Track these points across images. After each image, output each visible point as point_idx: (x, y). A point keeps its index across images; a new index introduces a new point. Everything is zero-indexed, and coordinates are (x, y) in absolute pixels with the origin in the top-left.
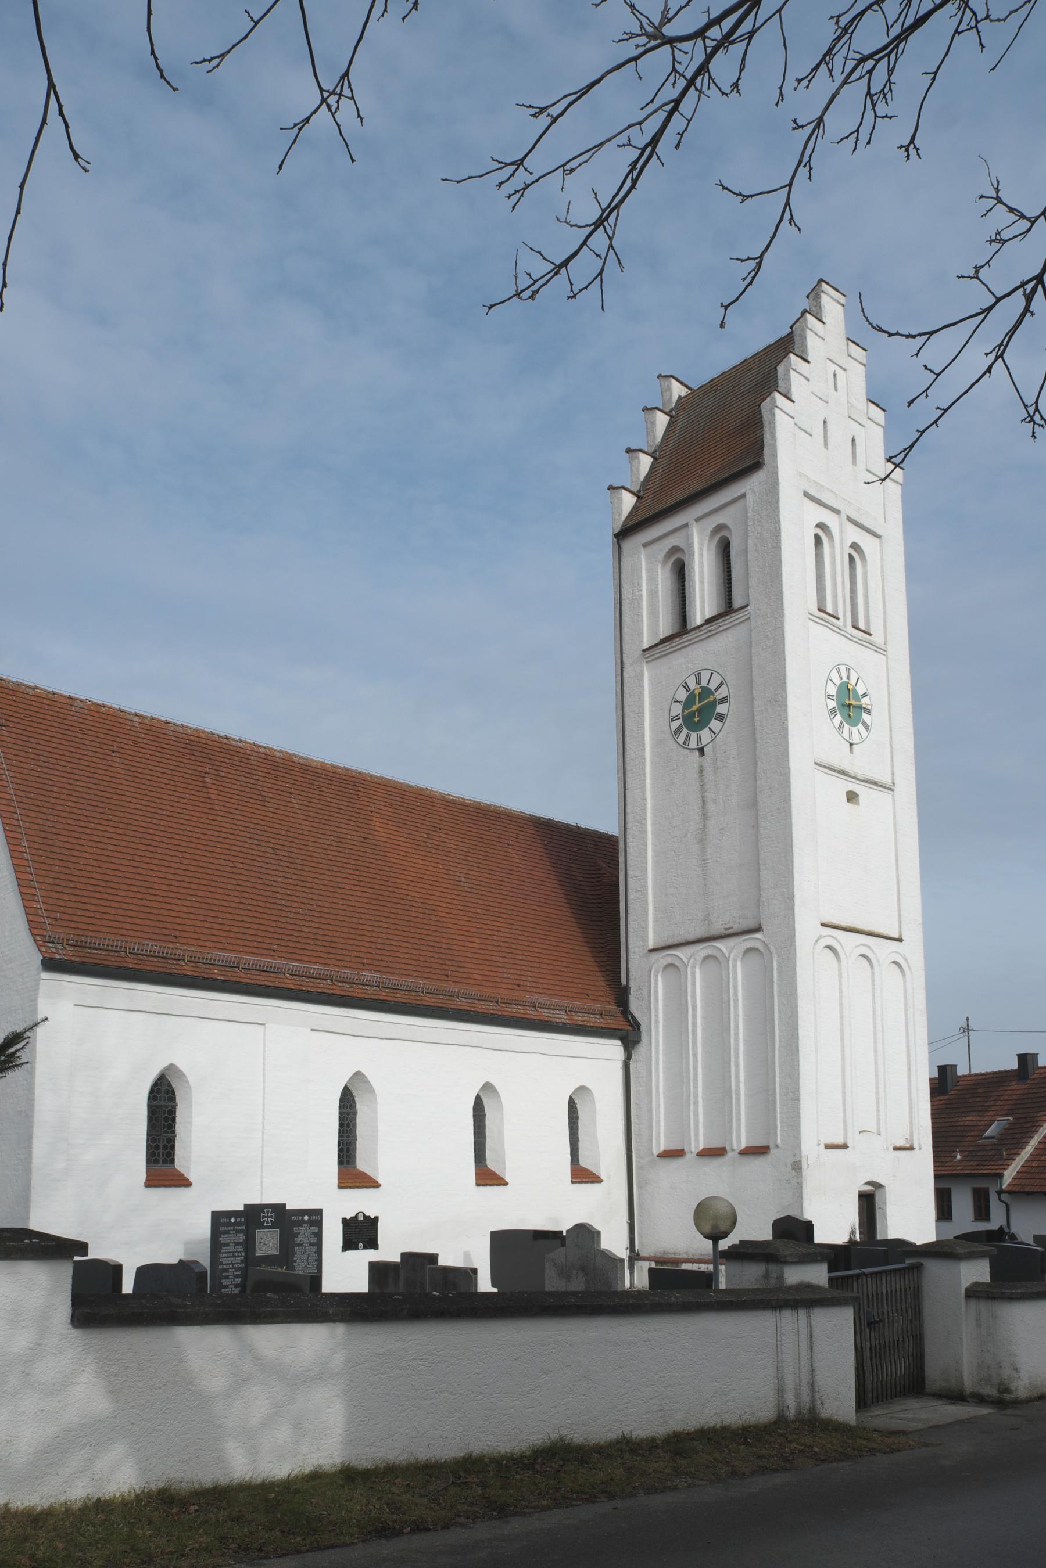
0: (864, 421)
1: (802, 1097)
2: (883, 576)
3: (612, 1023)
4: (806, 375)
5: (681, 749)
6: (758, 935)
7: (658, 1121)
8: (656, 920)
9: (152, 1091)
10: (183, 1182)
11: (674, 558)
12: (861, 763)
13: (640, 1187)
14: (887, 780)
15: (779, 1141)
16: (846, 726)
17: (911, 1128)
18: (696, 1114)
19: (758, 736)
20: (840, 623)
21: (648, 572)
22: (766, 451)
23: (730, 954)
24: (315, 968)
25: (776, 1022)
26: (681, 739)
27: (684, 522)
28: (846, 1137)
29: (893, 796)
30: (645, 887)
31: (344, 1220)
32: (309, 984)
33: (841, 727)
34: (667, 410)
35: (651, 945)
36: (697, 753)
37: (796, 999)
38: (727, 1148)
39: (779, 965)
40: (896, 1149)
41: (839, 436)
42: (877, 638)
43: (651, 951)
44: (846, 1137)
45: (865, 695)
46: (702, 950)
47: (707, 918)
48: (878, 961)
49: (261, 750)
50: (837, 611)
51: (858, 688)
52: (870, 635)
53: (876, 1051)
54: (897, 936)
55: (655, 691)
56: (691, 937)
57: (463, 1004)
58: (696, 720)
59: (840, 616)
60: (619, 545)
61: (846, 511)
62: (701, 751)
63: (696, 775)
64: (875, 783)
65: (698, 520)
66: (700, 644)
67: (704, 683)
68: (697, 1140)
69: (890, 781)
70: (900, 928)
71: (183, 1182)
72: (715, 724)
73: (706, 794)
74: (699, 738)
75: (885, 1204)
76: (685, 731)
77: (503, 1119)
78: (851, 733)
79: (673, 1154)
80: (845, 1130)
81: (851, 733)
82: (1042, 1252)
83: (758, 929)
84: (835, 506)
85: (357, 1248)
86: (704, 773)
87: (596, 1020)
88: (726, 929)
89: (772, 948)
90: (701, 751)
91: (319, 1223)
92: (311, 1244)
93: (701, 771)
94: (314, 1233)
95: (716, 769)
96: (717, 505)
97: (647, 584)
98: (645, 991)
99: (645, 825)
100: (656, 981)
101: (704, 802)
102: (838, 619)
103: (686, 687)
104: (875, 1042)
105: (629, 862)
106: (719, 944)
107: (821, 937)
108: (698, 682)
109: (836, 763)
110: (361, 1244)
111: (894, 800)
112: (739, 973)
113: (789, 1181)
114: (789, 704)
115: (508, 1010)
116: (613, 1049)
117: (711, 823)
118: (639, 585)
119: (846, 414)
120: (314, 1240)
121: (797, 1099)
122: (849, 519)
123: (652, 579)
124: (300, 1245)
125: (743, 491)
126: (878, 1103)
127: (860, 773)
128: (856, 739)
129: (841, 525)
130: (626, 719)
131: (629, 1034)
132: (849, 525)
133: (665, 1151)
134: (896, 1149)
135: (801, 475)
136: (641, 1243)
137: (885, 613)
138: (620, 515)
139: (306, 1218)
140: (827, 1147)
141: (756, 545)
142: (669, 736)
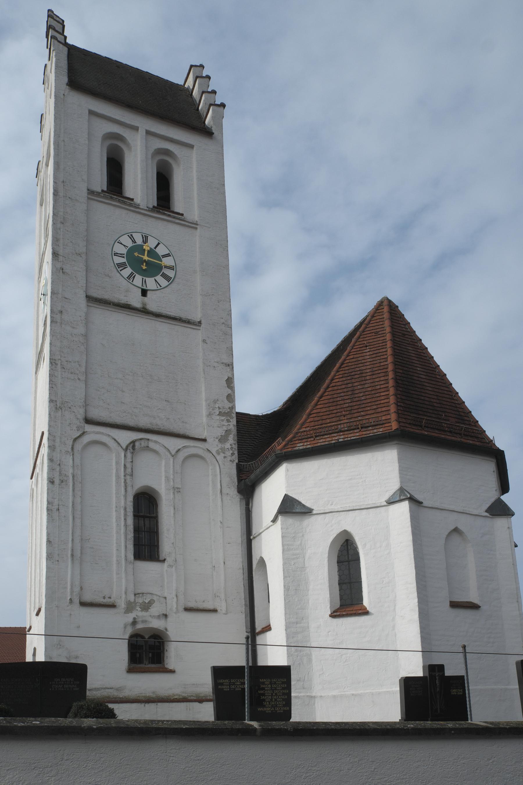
11: (108, 142)
33: (131, 277)
51: (158, 250)
78: (144, 282)
81: (144, 282)
140: (215, 611)
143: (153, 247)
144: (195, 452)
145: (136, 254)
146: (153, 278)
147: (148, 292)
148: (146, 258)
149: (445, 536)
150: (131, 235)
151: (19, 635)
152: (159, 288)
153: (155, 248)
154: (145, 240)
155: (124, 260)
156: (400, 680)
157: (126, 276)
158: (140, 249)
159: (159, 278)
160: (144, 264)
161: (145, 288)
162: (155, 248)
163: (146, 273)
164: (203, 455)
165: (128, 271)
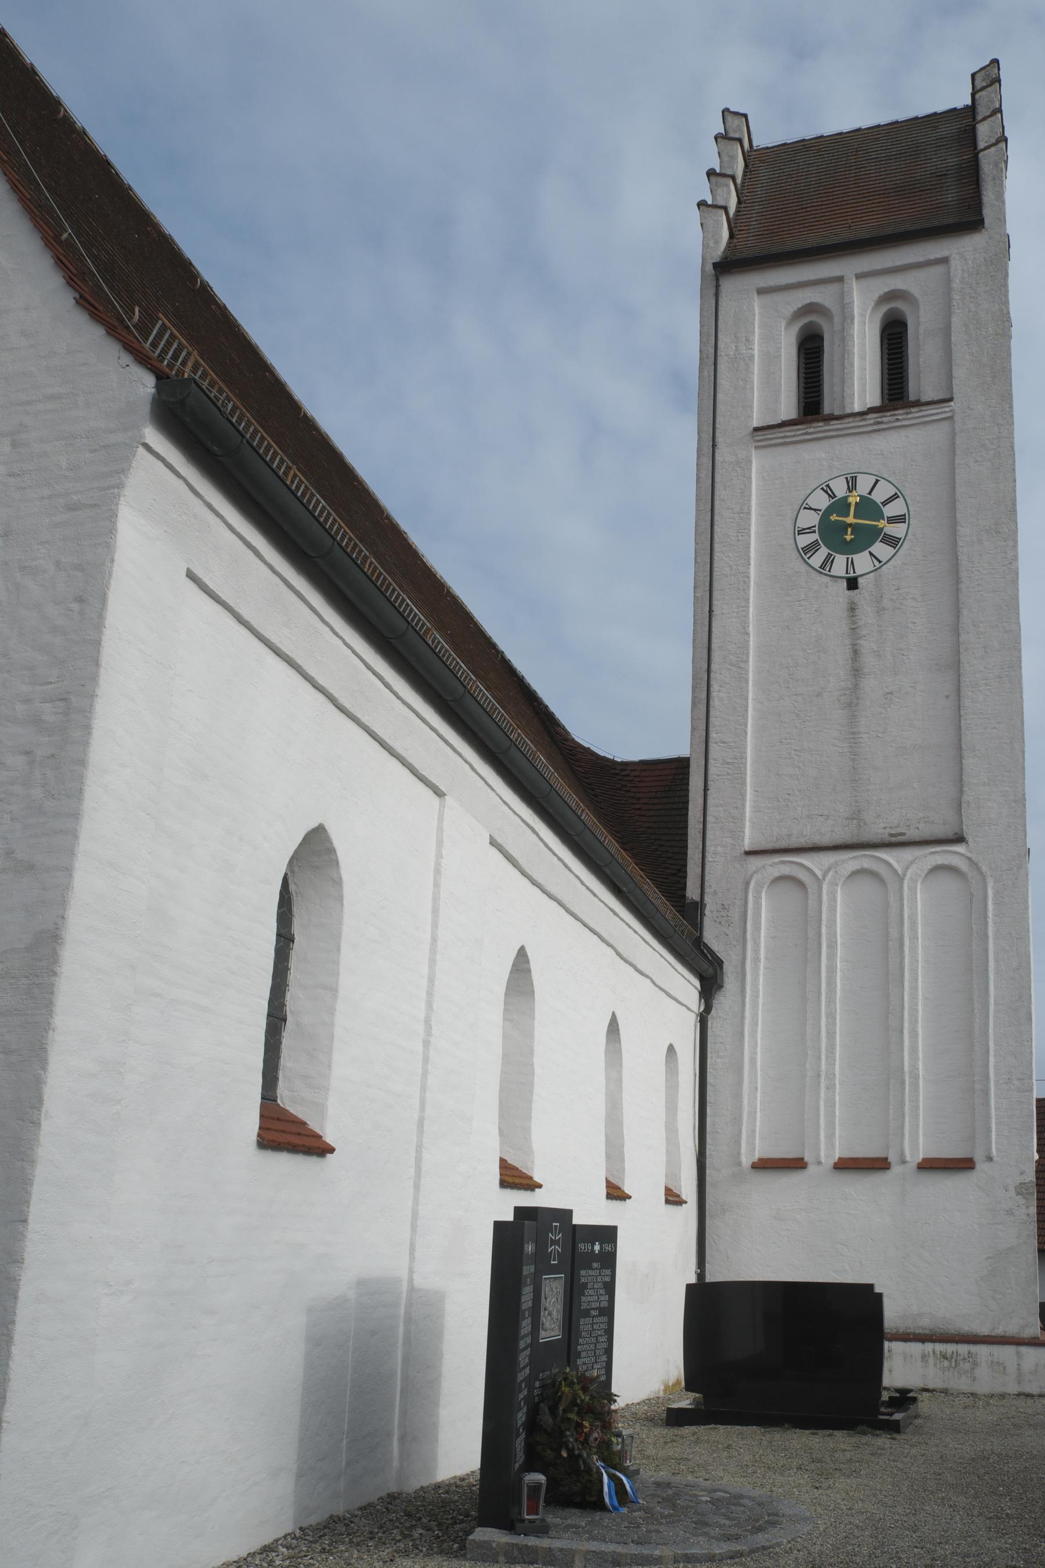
5: (814, 574)
6: (960, 848)
7: (753, 1113)
8: (756, 810)
11: (884, 308)
15: (994, 1152)
18: (831, 1104)
19: (963, 574)
21: (764, 324)
23: (825, 876)
26: (817, 560)
27: (838, 274)
30: (743, 757)
35: (747, 845)
38: (892, 1158)
39: (997, 893)
43: (748, 853)
47: (856, 815)
55: (780, 486)
56: (826, 841)
58: (848, 537)
60: (717, 280)
62: (852, 584)
65: (859, 276)
66: (857, 438)
68: (831, 1145)
73: (861, 642)
83: (959, 839)
86: (857, 612)
89: (984, 869)
90: (852, 584)
95: (880, 611)
96: (899, 263)
97: (760, 344)
98: (735, 914)
101: (856, 652)
103: (828, 491)
105: (712, 719)
113: (1010, 1212)
117: (869, 684)
125: (945, 253)
130: (716, 518)
133: (925, 1160)
138: (717, 242)
143: (865, 493)
144: (946, 862)
145: (834, 517)
146: (867, 552)
147: (860, 580)
148: (850, 519)
149: (846, 874)
150: (828, 486)
152: (878, 565)
154: (852, 484)
155: (815, 537)
157: (817, 565)
158: (841, 506)
160: (849, 530)
161: (852, 575)
162: (870, 493)
163: (850, 548)
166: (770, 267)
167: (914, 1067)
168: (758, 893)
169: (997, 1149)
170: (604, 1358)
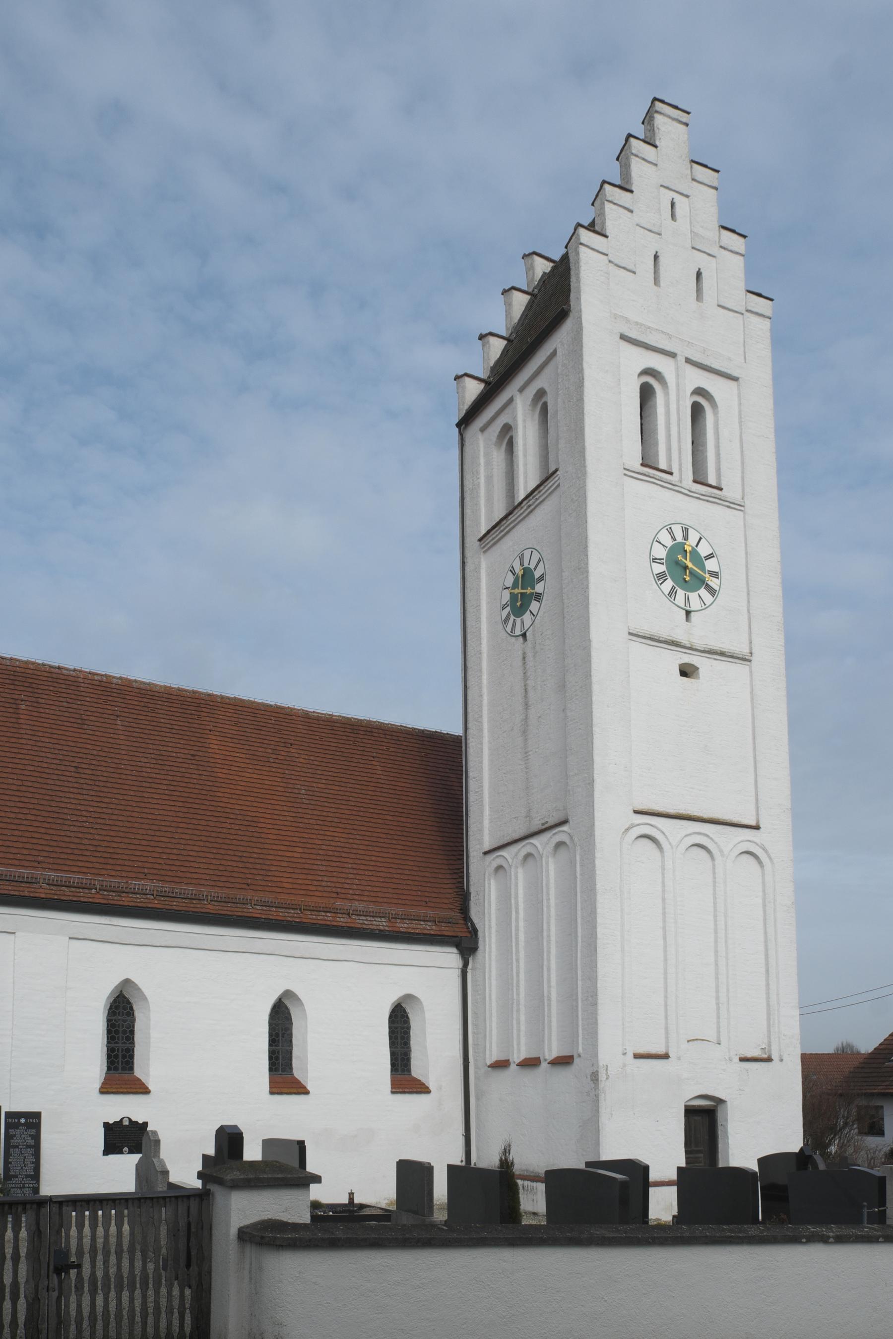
0: (715, 250)
1: (600, 1001)
2: (740, 422)
3: (446, 930)
4: (627, 206)
6: (565, 828)
9: (390, 1017)
10: (300, 1089)
12: (703, 631)
13: (478, 1098)
14: (742, 649)
15: (580, 1050)
16: (681, 593)
17: (769, 1037)
20: (673, 479)
22: (573, 296)
24: (75, 878)
25: (579, 920)
28: (667, 1047)
29: (750, 667)
31: (106, 1125)
32: (67, 894)
33: (672, 593)
34: (530, 290)
36: (521, 639)
37: (595, 895)
38: (542, 1059)
40: (743, 1060)
41: (678, 269)
42: (731, 492)
43: (486, 853)
44: (667, 1047)
45: (710, 556)
46: (522, 849)
48: (721, 851)
49: (96, 678)
50: (670, 466)
51: (699, 549)
52: (721, 489)
53: (716, 952)
54: (753, 823)
56: (516, 836)
57: (256, 911)
59: (675, 470)
61: (683, 352)
63: (520, 664)
64: (722, 654)
67: (526, 565)
68: (550, 1050)
69: (748, 651)
70: (758, 814)
71: (300, 1089)
72: (534, 606)
74: (522, 622)
75: (726, 1120)
76: (512, 617)
77: (307, 1026)
78: (687, 599)
79: (501, 1065)
80: (667, 1038)
81: (687, 599)
82: (623, 1184)
83: (564, 822)
84: (668, 348)
85: (120, 1152)
87: (428, 927)
88: (543, 824)
90: (524, 635)
91: (37, 1126)
92: (28, 1147)
93: (524, 658)
94: (30, 1136)
99: (481, 722)
100: (489, 884)
101: (526, 691)
102: (671, 474)
104: (716, 941)
106: (533, 841)
107: (632, 826)
108: (522, 564)
109: (664, 633)
110: (126, 1149)
111: (751, 672)
112: (551, 868)
113: (588, 1094)
114: (591, 570)
115: (310, 917)
116: (449, 957)
118: (478, 473)
119: (689, 246)
120: (31, 1142)
121: (595, 1004)
122: (688, 361)
123: (488, 464)
124: (16, 1147)
126: (718, 1009)
127: (699, 643)
128: (695, 604)
129: (677, 369)
131: (467, 944)
132: (689, 369)
133: (526, 1059)
134: (743, 1060)
135: (616, 316)
136: (478, 1157)
137: (743, 463)
138: (464, 403)
139: (23, 1121)
140: (637, 1056)
141: (564, 402)
142: (500, 626)
146: (696, 593)
151: (25, 1126)
152: (704, 607)
153: (697, 546)
156: (236, 1127)
159: (703, 592)
161: (688, 608)
162: (697, 546)
164: (663, 846)
165: (669, 584)
166: (516, 374)
167: (549, 992)
168: (489, 880)
169: (583, 1049)
170: (32, 1159)
